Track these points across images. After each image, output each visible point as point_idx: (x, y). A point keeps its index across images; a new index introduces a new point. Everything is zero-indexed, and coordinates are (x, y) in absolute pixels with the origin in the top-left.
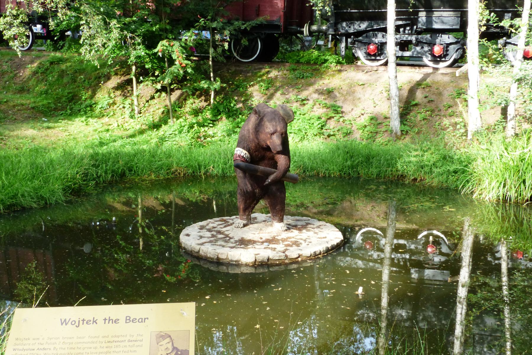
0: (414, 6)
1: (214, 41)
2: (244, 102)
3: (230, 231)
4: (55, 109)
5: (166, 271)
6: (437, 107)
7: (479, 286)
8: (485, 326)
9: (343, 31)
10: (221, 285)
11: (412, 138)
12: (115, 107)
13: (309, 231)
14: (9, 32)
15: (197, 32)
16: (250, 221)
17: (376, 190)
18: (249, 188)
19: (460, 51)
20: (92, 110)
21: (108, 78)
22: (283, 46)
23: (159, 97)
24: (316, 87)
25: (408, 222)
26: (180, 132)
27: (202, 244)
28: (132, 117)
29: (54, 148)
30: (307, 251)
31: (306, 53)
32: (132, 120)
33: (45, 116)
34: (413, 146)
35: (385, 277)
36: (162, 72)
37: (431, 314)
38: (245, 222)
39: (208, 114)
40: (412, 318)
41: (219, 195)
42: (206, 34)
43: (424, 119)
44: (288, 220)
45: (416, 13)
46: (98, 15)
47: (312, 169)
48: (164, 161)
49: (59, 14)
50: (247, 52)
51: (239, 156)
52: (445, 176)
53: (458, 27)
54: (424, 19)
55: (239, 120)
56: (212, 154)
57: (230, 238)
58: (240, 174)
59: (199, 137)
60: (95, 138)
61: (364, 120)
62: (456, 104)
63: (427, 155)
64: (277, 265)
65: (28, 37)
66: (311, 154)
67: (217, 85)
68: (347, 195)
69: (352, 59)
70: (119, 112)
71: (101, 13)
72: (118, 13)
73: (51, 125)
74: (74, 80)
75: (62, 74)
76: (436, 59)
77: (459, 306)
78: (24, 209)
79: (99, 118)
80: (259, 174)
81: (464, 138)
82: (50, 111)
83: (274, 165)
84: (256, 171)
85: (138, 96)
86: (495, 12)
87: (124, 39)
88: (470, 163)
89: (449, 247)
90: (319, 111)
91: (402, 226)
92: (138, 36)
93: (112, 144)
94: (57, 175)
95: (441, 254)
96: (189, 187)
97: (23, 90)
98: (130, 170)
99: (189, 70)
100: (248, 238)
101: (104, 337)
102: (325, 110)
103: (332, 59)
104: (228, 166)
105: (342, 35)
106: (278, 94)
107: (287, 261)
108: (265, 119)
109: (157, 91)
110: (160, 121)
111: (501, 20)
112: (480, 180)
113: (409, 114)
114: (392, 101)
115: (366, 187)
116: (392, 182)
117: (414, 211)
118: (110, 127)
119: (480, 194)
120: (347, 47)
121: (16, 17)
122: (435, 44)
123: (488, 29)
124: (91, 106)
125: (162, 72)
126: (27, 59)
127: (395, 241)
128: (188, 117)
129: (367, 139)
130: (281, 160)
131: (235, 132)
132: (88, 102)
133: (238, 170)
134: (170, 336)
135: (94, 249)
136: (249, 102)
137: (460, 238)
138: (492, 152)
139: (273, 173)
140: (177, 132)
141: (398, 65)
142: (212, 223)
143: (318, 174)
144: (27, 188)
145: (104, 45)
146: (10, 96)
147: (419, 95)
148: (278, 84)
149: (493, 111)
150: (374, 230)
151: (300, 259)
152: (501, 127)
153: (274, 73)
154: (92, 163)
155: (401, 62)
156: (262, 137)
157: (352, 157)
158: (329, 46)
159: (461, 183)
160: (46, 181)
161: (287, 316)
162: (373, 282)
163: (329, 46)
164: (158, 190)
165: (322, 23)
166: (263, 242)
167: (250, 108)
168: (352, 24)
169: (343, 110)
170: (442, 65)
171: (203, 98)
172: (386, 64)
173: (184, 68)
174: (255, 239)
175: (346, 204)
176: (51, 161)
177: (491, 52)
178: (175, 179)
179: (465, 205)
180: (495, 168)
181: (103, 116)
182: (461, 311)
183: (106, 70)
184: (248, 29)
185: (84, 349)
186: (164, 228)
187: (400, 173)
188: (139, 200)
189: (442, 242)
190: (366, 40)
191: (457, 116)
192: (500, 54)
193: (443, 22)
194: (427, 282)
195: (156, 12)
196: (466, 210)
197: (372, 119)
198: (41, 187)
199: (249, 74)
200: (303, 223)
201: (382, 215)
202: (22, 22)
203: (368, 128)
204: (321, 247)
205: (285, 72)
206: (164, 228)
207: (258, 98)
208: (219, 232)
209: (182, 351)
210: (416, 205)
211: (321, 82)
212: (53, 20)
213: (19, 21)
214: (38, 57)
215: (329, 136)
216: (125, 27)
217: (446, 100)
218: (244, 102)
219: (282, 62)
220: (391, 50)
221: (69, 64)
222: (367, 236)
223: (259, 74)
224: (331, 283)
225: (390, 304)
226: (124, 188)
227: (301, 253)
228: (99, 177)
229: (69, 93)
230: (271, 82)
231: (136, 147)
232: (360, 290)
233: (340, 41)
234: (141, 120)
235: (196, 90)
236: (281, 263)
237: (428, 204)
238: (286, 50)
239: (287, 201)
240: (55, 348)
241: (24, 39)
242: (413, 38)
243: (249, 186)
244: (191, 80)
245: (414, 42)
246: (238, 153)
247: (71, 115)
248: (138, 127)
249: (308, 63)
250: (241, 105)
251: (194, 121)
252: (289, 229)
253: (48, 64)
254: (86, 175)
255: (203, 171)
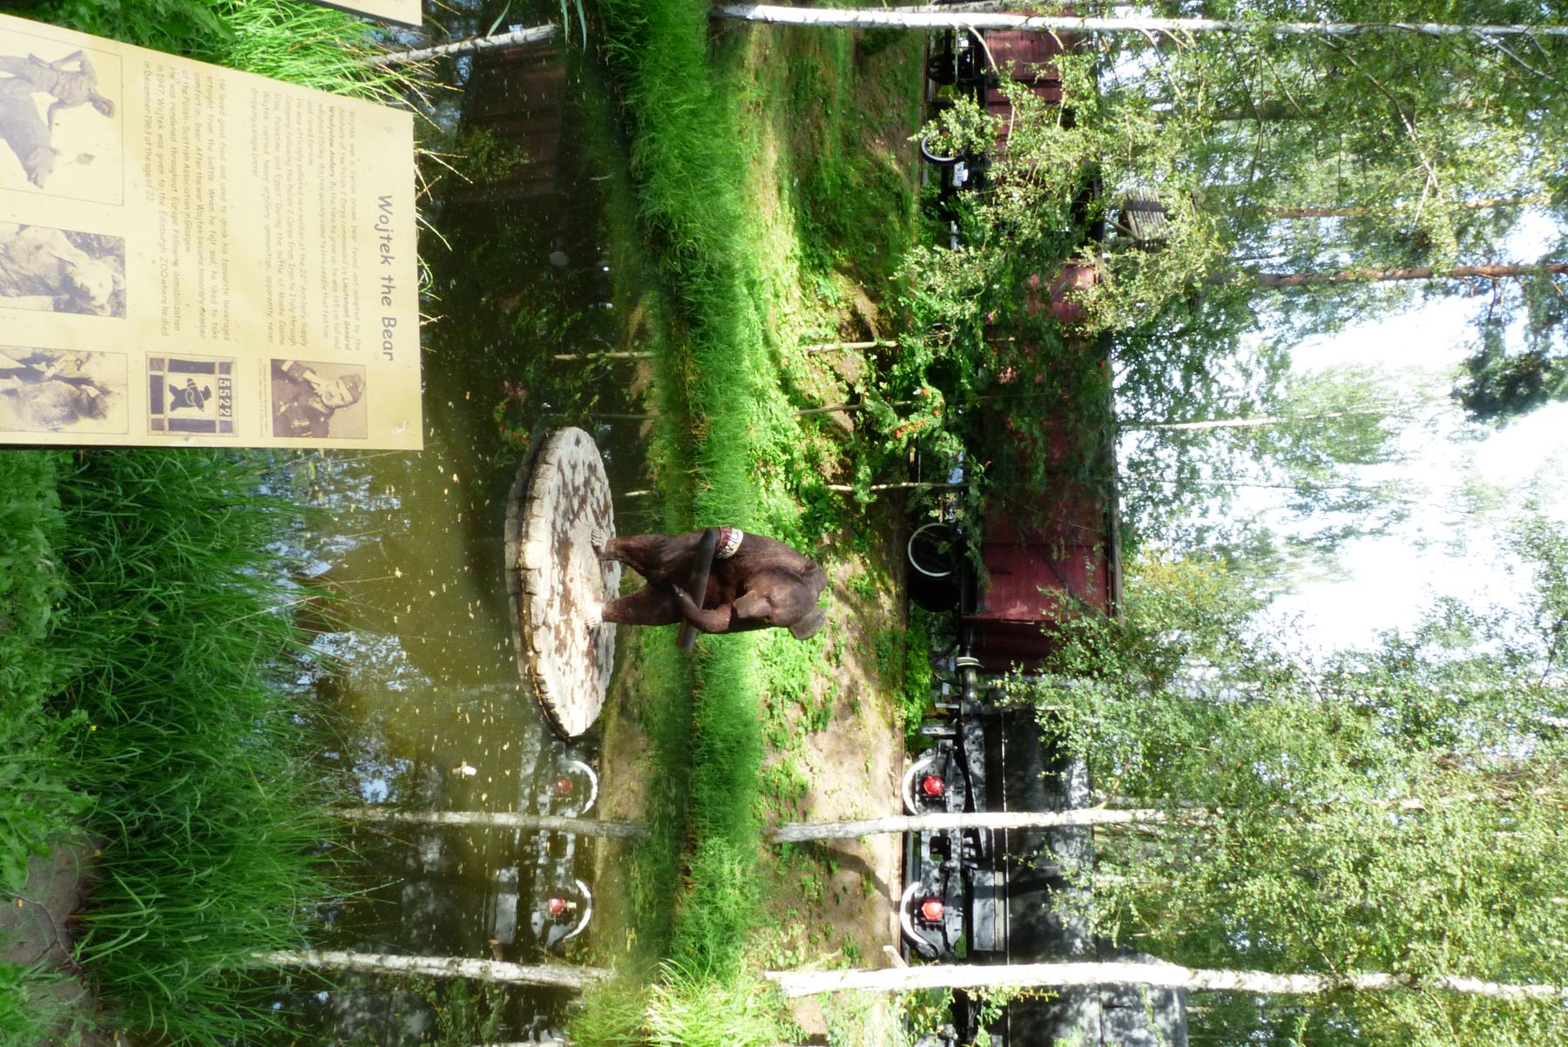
0: (1013, 864)
1: (944, 491)
2: (832, 548)
3: (587, 519)
4: (814, 202)
5: (513, 404)
6: (825, 911)
7: (483, 998)
8: (404, 1014)
9: (966, 729)
10: (479, 502)
11: (767, 865)
12: (821, 310)
13: (587, 670)
14: (952, 121)
15: (961, 459)
16: (604, 558)
17: (668, 799)
18: (668, 556)
19: (932, 953)
20: (814, 268)
21: (874, 297)
22: (939, 619)
23: (841, 390)
24: (863, 682)
25: (606, 860)
26: (774, 428)
27: (560, 469)
28: (802, 340)
29: (742, 199)
30: (547, 668)
31: (924, 661)
32: (796, 340)
33: (801, 184)
34: (752, 867)
35: (501, 819)
36: (885, 395)
37: (431, 907)
38: (603, 549)
39: (808, 480)
40: (417, 875)
41: (658, 501)
42: (956, 476)
43: (803, 887)
44: (609, 632)
45: (1001, 867)
46: (986, 278)
47: (707, 676)
48: (721, 399)
49: (984, 209)
50: (925, 552)
51: (727, 538)
52: (694, 930)
53: (976, 947)
54: (991, 883)
55: (799, 538)
56: (734, 488)
57: (572, 522)
58: (694, 539)
59: (766, 463)
60: (761, 273)
61: (801, 773)
62: (832, 949)
63: (733, 894)
64: (520, 610)
65: (945, 154)
66: (735, 673)
67: (863, 497)
68: (656, 742)
69: (914, 746)
70: (810, 316)
71: (989, 284)
72: (992, 315)
73: (786, 193)
74: (868, 236)
75: (879, 215)
76: (916, 907)
77: (445, 962)
78: (627, 142)
79: (800, 280)
80: (694, 575)
81: (768, 965)
82: (811, 193)
83: (711, 604)
84: (700, 570)
85: (841, 350)
86: (1004, 1018)
87: (943, 323)
88: (718, 977)
89: (556, 942)
90: (817, 688)
91: (601, 850)
92: (950, 350)
93: (751, 302)
94: (691, 202)
95: (547, 925)
96: (672, 444)
97: (849, 145)
98: (702, 336)
99: (889, 445)
100: (572, 556)
101: (355, 276)
102: (820, 698)
103: (915, 709)
104: (713, 517)
105: (959, 728)
106: (850, 612)
107: (527, 629)
108: (796, 586)
109: (851, 387)
110: (796, 391)
111: (989, 1028)
112: (687, 997)
113: (813, 857)
114: (836, 826)
115: (673, 780)
116: (684, 828)
117: (626, 872)
118: (783, 300)
119: (658, 998)
120: (936, 737)
121: (980, 132)
122: (943, 904)
123: (973, 1004)
124: (821, 266)
125: (885, 395)
126: (905, 153)
127: (571, 837)
128: (804, 443)
129: (765, 780)
130: (722, 617)
131: (776, 530)
132: (829, 261)
133: (700, 536)
134: (355, 401)
135: (557, 271)
136: (832, 557)
137: (574, 962)
138: (740, 1020)
139: (695, 597)
140: (774, 422)
141: (905, 835)
142: (602, 488)
143: (697, 687)
144: (667, 147)
145: (931, 289)
146: (838, 120)
147: (849, 877)
148: (866, 610)
149: (819, 1018)
150: (594, 796)
151: (531, 653)
152: (788, 1035)
153: (886, 602)
154: (716, 266)
155: (910, 841)
156: (764, 581)
157: (730, 750)
158: (938, 705)
159: (679, 961)
160: (680, 183)
161: (419, 631)
162: (484, 797)
163: (938, 705)
164: (664, 388)
165: (979, 691)
166: (563, 583)
167: (821, 559)
168: (980, 749)
169: (820, 733)
170: (905, 918)
171: (840, 471)
172: (906, 812)
173: (893, 436)
174: (570, 569)
175: (642, 741)
176: (717, 193)
177: (929, 1011)
178: (687, 420)
179: (639, 970)
180: (709, 1025)
181: (804, 288)
182: (435, 965)
183: (887, 293)
184: (968, 554)
185: (332, 239)
186: (597, 398)
187: (700, 843)
188: (646, 354)
189: (570, 926)
190: (949, 773)
191: (809, 950)
192: (926, 1029)
193: (984, 918)
194: (492, 900)
195: (993, 385)
196: (629, 972)
197: (803, 787)
198: (667, 173)
199: (884, 557)
200: (602, 660)
201: (620, 811)
202: (971, 142)
203: (786, 781)
204: (553, 694)
205: (890, 623)
206: (597, 398)
207: (841, 574)
208: (583, 501)
209: (326, 424)
210: (638, 876)
211: (871, 690)
212: (975, 199)
213: (974, 138)
214: (909, 171)
215: (770, 707)
216: (965, 327)
217: (837, 929)
218: (832, 548)
219: (908, 617)
220: (934, 822)
221: (897, 226)
222: (581, 783)
223: (885, 574)
224: (483, 716)
225: (452, 828)
226: (668, 324)
227: (543, 655)
228: (689, 279)
229: (844, 226)
230: (870, 598)
231: (746, 346)
232: (469, 770)
233: (948, 726)
234: (797, 357)
235: (853, 458)
236: (523, 618)
237: (640, 897)
238: (931, 625)
239: (647, 629)
240: (334, 184)
241: (941, 147)
242: (955, 863)
243: (671, 556)
244: (872, 447)
245: (947, 865)
246: (733, 536)
247: (805, 229)
248: (784, 351)
249: (907, 666)
250: (827, 541)
251: (796, 455)
252: (590, 632)
253: (897, 189)
254: (693, 255)
255: (702, 471)
